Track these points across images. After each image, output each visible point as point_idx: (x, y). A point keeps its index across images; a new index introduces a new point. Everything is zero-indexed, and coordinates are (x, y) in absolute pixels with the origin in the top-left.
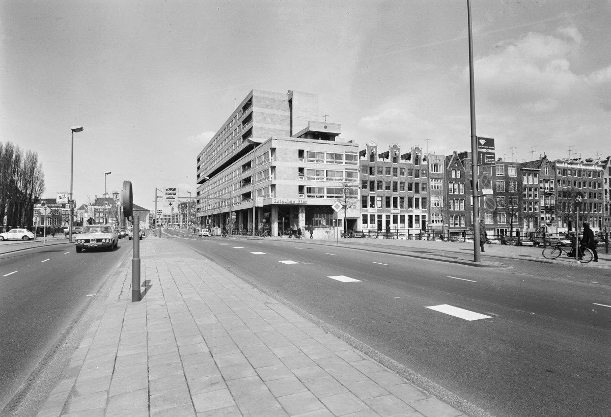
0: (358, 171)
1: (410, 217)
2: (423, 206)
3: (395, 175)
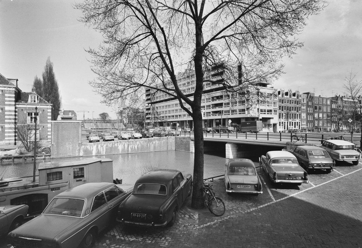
0: (277, 102)
1: (295, 123)
2: (299, 118)
3: (282, 103)
